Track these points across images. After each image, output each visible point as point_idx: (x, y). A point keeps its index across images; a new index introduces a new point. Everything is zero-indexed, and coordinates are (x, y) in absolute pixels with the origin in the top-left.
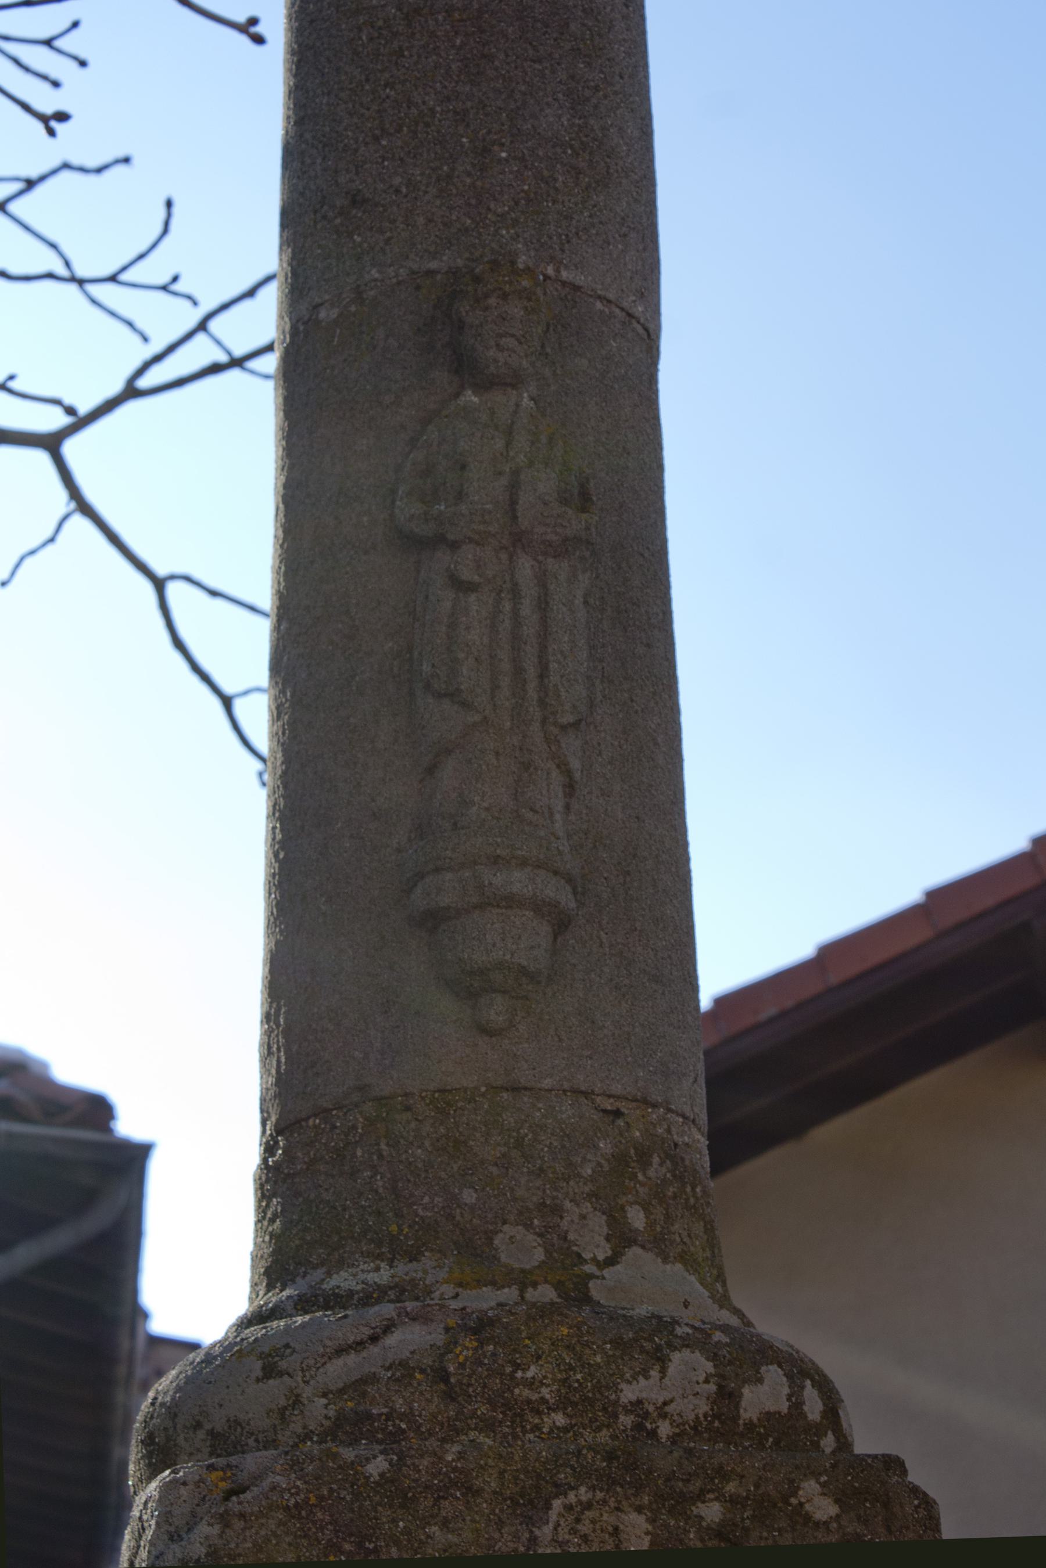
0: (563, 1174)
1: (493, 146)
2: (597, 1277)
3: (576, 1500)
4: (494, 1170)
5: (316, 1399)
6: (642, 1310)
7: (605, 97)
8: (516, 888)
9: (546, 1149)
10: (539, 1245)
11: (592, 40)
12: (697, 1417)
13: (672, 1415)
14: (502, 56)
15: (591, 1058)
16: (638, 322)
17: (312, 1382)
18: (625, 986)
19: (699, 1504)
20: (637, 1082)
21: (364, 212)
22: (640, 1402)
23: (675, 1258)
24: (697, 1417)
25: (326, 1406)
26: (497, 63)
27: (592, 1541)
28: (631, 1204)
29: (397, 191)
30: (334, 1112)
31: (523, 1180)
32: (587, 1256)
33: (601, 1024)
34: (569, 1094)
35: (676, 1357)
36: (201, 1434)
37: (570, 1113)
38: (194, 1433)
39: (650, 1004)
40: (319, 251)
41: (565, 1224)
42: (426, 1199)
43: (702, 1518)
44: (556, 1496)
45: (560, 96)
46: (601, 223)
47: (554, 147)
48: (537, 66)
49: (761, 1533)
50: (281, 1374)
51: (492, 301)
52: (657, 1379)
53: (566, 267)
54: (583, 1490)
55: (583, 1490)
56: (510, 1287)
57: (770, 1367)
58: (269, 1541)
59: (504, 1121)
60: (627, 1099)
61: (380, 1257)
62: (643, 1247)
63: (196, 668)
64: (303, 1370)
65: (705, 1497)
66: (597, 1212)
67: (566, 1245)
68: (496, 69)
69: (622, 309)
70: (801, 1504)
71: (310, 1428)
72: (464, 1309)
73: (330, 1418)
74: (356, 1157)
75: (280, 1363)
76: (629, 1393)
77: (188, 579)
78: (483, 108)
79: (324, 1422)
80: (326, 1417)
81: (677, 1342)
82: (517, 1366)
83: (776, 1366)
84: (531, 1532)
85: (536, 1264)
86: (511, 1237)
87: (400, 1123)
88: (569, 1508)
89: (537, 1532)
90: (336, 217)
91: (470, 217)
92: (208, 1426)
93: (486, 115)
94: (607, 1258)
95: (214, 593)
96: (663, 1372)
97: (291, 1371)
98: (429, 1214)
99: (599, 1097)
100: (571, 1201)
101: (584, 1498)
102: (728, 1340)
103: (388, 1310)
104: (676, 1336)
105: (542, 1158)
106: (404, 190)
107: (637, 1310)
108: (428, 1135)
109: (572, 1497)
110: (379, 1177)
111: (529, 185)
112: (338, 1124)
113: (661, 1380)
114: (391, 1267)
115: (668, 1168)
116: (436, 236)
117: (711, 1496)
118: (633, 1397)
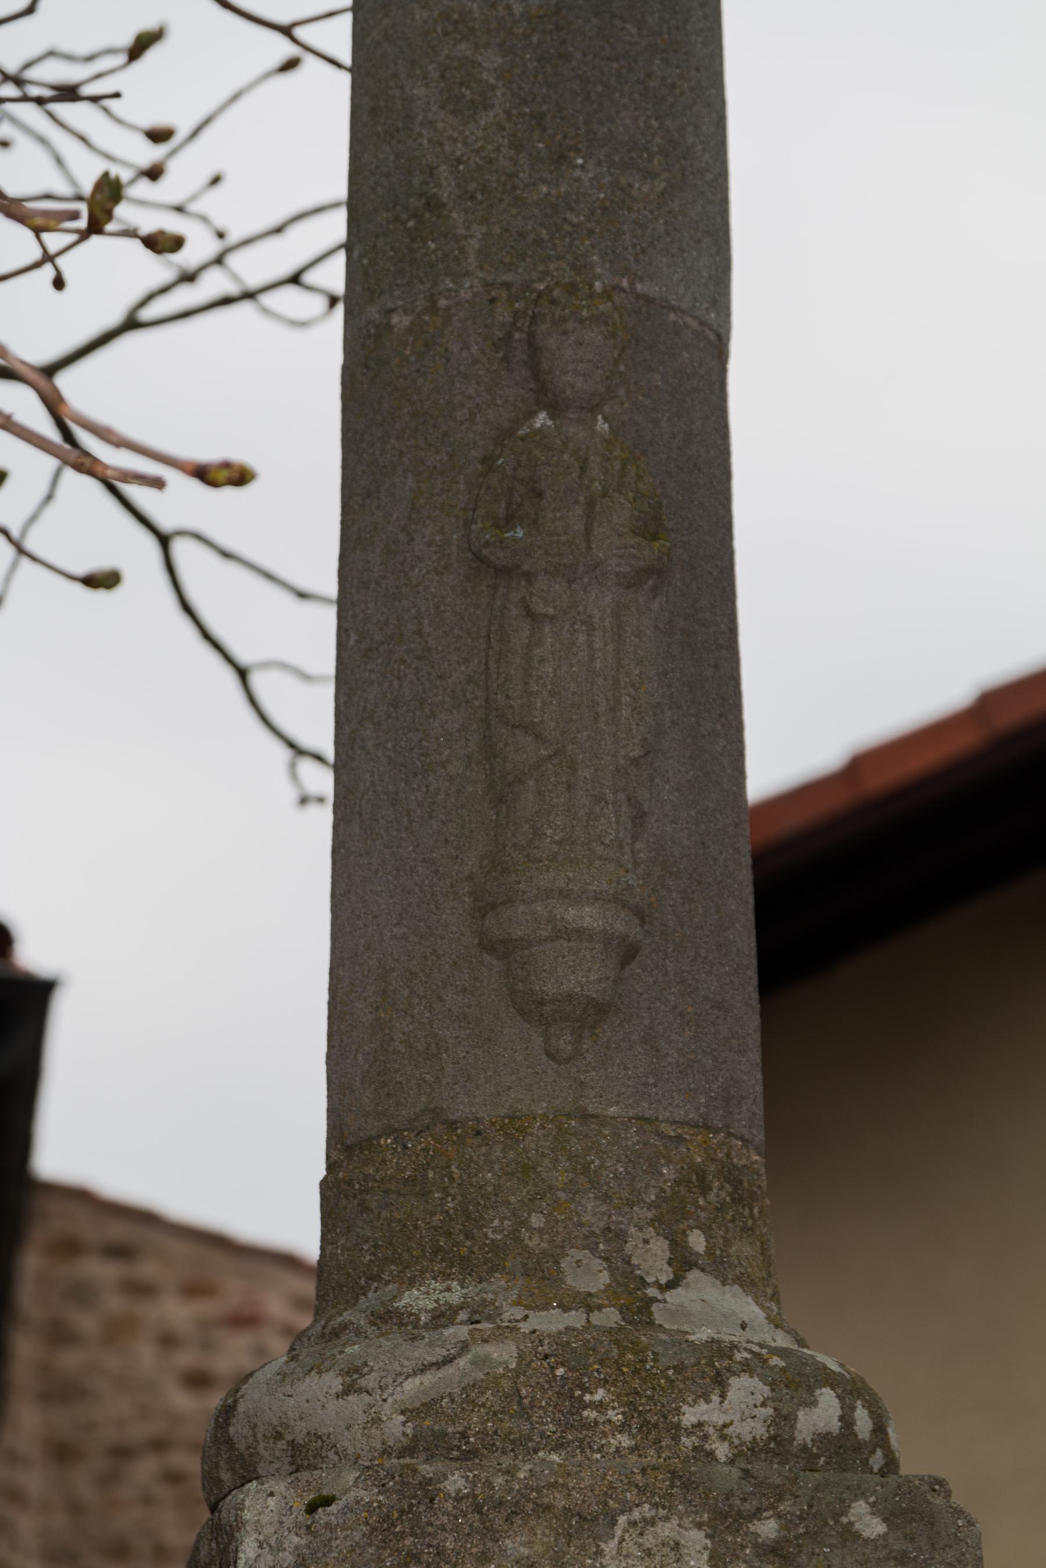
0: (627, 1199)
1: (569, 151)
2: (660, 1301)
3: (640, 1517)
4: (562, 1195)
5: (394, 1416)
6: (702, 1335)
7: (682, 94)
8: (587, 922)
9: (611, 1175)
10: (605, 1269)
11: (669, 34)
12: (754, 1438)
13: (731, 1437)
14: (578, 56)
15: (655, 1086)
16: (711, 329)
17: (390, 1400)
18: (689, 1013)
19: (755, 1522)
20: (699, 1109)
21: (439, 217)
22: (700, 1425)
23: (733, 1279)
24: (754, 1438)
25: (404, 1424)
26: (574, 63)
27: (654, 1554)
28: (691, 1228)
29: (472, 197)
30: (406, 1133)
31: (589, 1206)
32: (650, 1279)
33: (666, 1052)
34: (633, 1121)
35: (734, 1382)
36: (282, 1445)
37: (634, 1139)
38: (274, 1443)
39: (713, 1030)
40: (392, 253)
41: (629, 1248)
42: (496, 1223)
43: (758, 1535)
44: (622, 1512)
45: (636, 96)
46: (675, 230)
47: (630, 151)
48: (615, 65)
49: (813, 1549)
50: (360, 1391)
51: (569, 325)
52: (718, 1403)
53: (641, 279)
54: (647, 1506)
55: (647, 1506)
56: (577, 1310)
57: (824, 1390)
58: (354, 1551)
59: (571, 1147)
60: (690, 1125)
61: (448, 1277)
62: (703, 1270)
63: (207, 636)
64: (381, 1388)
65: (761, 1515)
66: (659, 1237)
67: (629, 1270)
68: (573, 70)
69: (695, 318)
70: (851, 1523)
71: (389, 1443)
72: (534, 1332)
73: (408, 1435)
74: (427, 1178)
75: (359, 1381)
76: (690, 1416)
77: (198, 537)
78: (559, 112)
79: (402, 1439)
80: (404, 1434)
81: (736, 1367)
82: (585, 1390)
83: (829, 1388)
84: (598, 1546)
85: (602, 1287)
86: (578, 1261)
87: (471, 1147)
88: (633, 1524)
89: (603, 1546)
90: (409, 219)
91: (545, 228)
92: (290, 1438)
93: (563, 119)
94: (669, 1281)
95: (226, 555)
96: (723, 1396)
97: (370, 1389)
98: (499, 1237)
99: (663, 1124)
100: (635, 1226)
101: (648, 1515)
102: (784, 1364)
103: (462, 1332)
104: (735, 1362)
105: (608, 1184)
106: (479, 196)
107: (698, 1335)
108: (498, 1159)
109: (636, 1515)
110: (450, 1199)
111: (605, 193)
112: (410, 1145)
113: (720, 1404)
114: (463, 1288)
115: (727, 1192)
116: (512, 247)
117: (766, 1514)
118: (694, 1420)
